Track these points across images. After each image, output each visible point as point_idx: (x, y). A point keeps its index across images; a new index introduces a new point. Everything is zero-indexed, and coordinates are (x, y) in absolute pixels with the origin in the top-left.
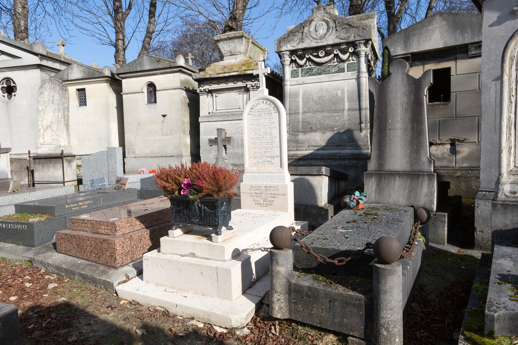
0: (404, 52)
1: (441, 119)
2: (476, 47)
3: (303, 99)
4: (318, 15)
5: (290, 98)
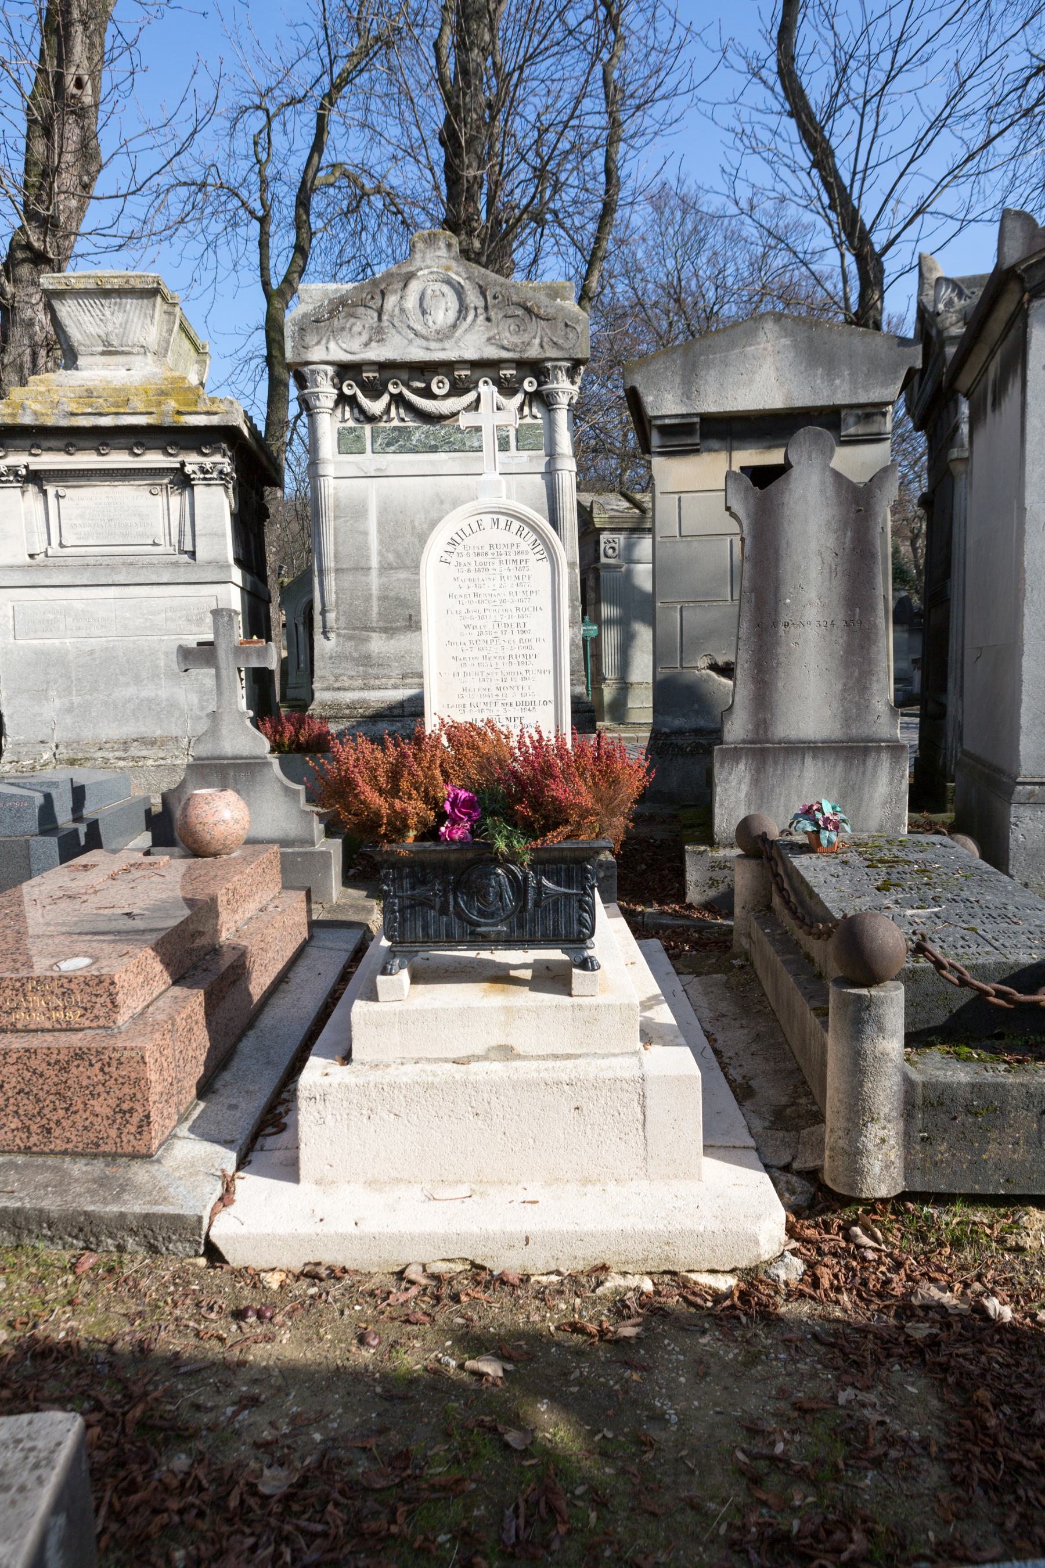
0: (683, 410)
2: (858, 417)
3: (380, 524)
4: (429, 262)
5: (336, 518)
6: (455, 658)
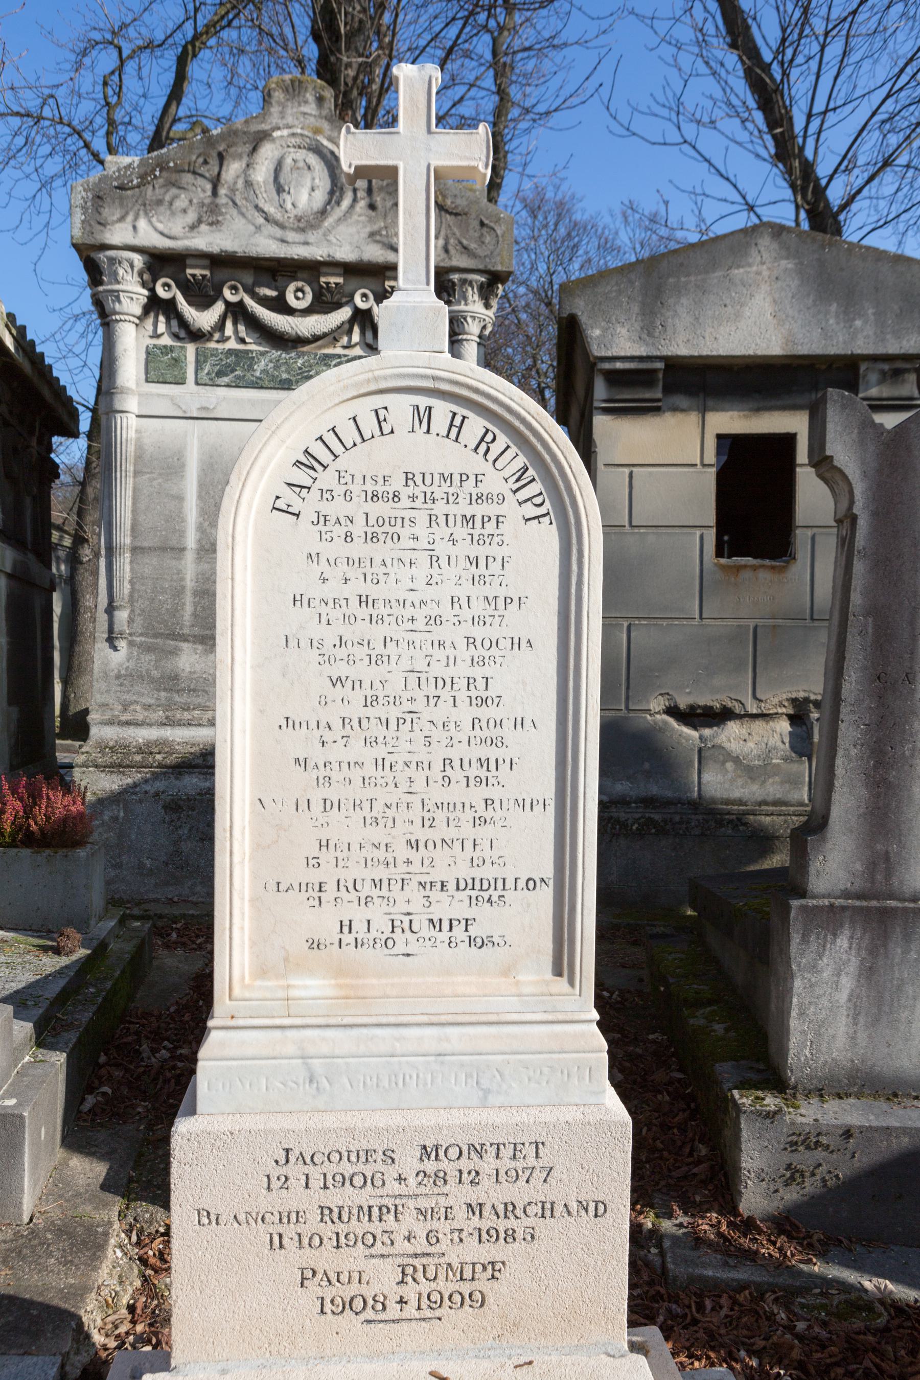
0: (642, 351)
1: (760, 622)
2: (883, 373)
3: (202, 486)
4: (290, 120)
5: (136, 473)
6: (302, 763)
